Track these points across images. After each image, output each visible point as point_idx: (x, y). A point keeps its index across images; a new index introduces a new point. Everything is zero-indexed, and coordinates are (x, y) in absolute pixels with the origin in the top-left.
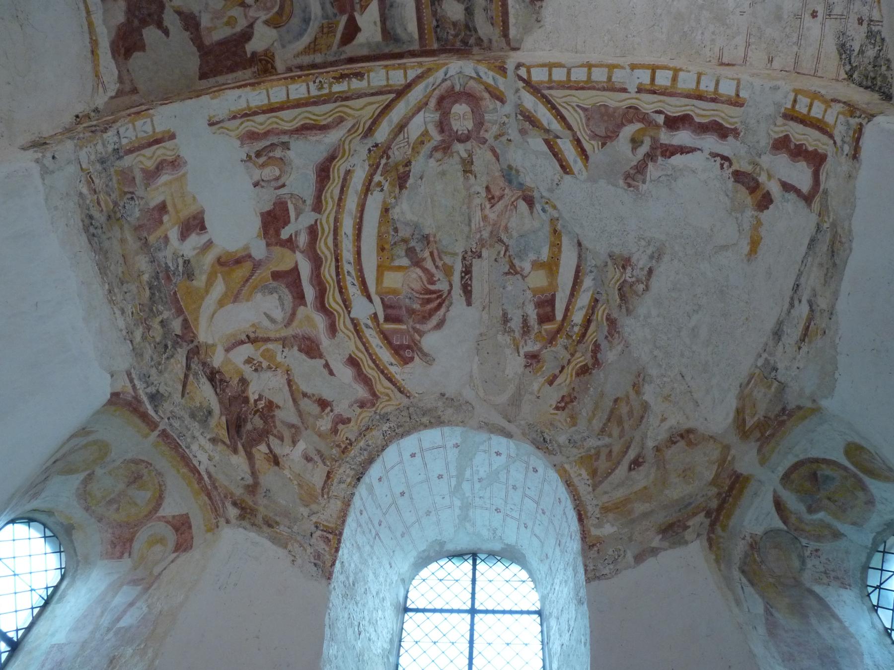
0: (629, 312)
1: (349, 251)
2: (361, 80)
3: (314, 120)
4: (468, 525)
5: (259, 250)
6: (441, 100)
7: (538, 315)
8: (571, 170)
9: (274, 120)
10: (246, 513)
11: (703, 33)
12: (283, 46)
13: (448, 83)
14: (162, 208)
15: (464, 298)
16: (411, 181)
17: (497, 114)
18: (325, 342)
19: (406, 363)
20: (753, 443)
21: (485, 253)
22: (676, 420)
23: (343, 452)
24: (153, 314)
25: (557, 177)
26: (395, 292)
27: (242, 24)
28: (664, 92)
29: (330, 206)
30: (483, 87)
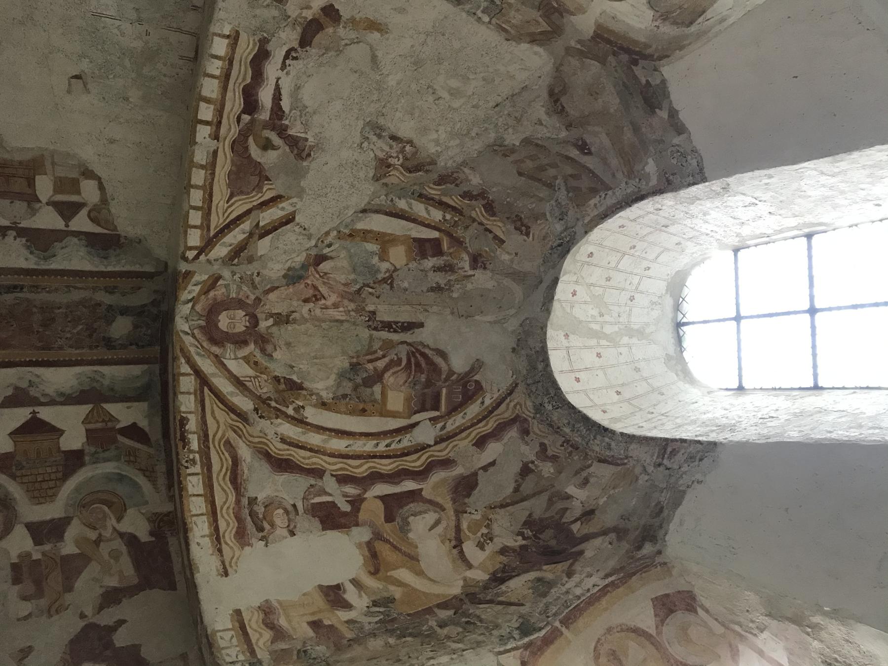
0: (433, 163)
1: (365, 445)
2: (188, 420)
3: (227, 470)
4: (648, 331)
5: (362, 534)
6: (213, 341)
7: (433, 256)
8: (291, 214)
9: (224, 511)
10: (651, 533)
11: (165, 75)
12: (147, 503)
13: (196, 331)
14: (315, 625)
15: (416, 330)
16: (294, 378)
17: (230, 284)
18: (458, 471)
19: (481, 388)
20: (565, 20)
21: (371, 308)
22: (539, 111)
23: (577, 448)
24: (431, 635)
25: (297, 229)
26: (408, 400)
27: (118, 544)
28: (220, 112)
29: (318, 461)
30: (203, 297)
